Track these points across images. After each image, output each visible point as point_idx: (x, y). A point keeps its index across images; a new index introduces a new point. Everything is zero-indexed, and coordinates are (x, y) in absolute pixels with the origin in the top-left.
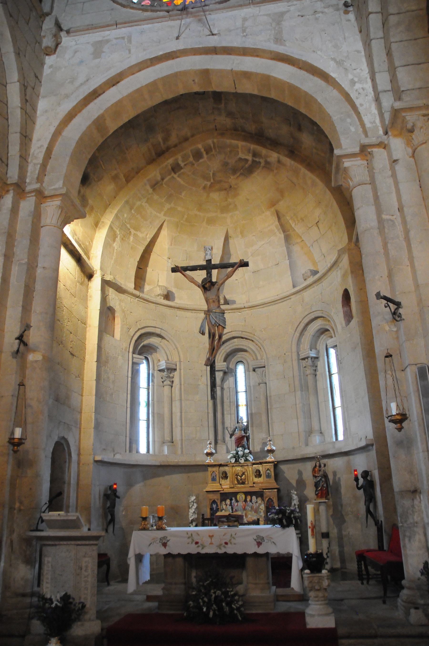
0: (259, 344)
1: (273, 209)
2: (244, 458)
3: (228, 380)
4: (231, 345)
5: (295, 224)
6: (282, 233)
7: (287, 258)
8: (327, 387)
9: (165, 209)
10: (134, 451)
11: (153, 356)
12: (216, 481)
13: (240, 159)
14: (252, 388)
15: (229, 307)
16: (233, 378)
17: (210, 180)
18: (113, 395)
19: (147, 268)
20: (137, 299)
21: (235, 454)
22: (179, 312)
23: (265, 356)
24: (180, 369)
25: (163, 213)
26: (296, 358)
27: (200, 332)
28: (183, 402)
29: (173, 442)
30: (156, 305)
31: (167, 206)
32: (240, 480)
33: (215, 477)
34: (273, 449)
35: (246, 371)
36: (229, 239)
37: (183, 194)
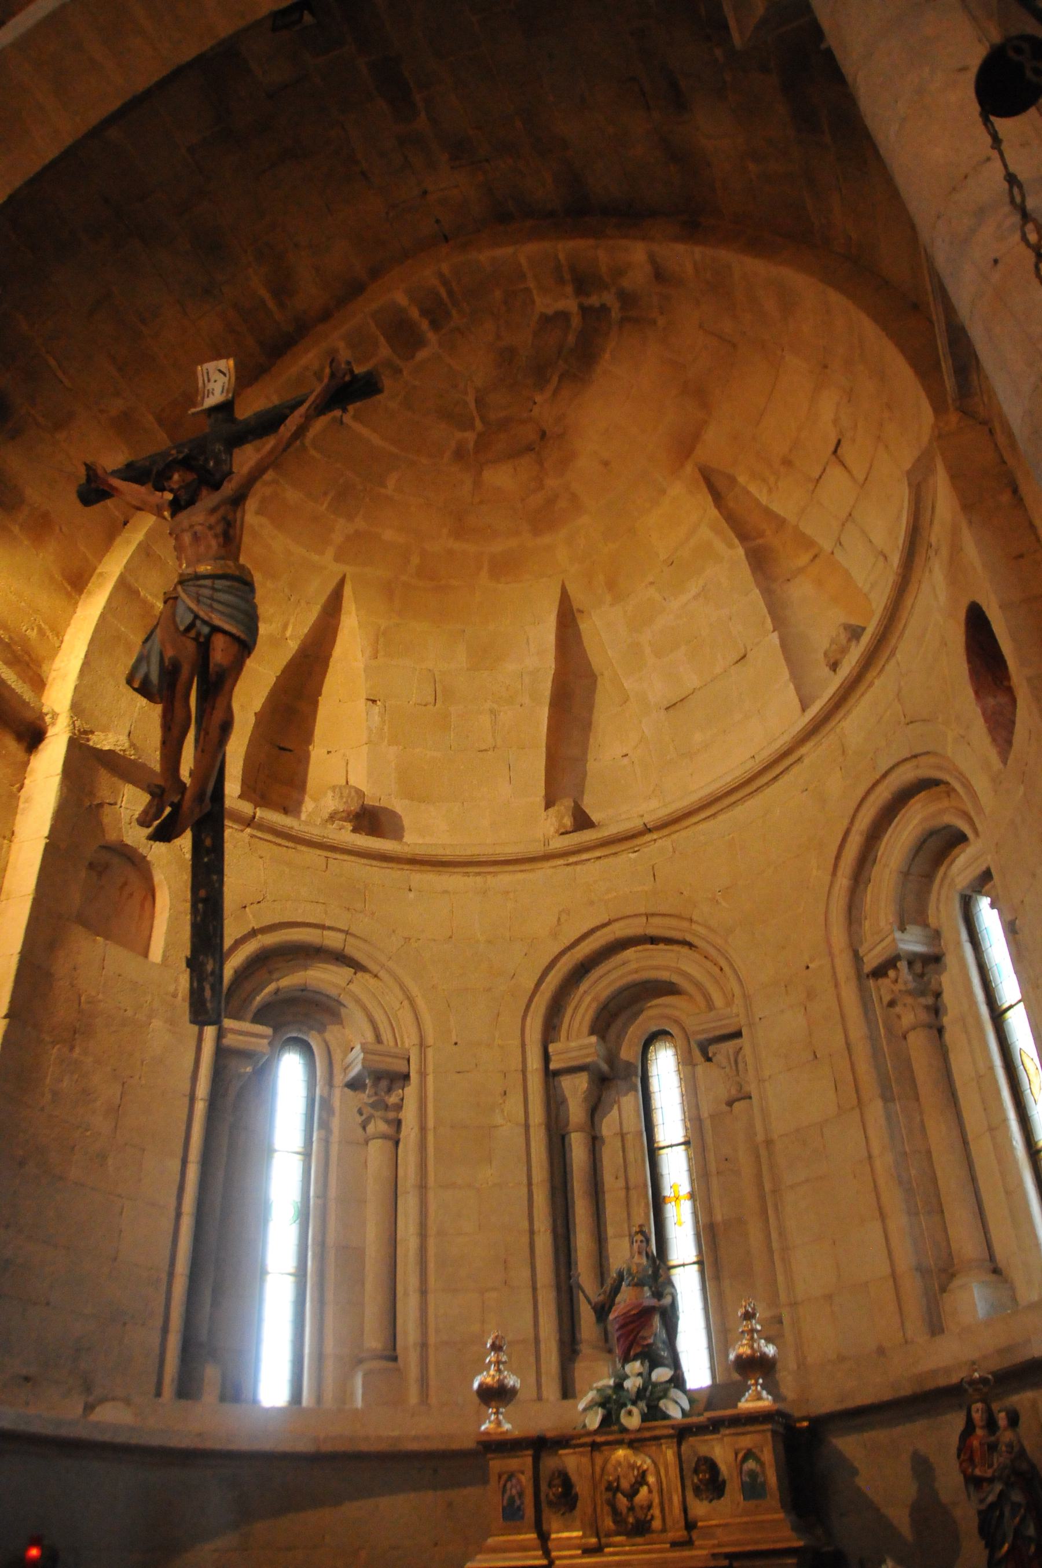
0: (713, 953)
1: (689, 468)
2: (642, 1405)
3: (616, 1107)
4: (613, 976)
5: (770, 491)
6: (736, 541)
7: (769, 624)
8: (991, 1068)
9: (338, 538)
10: (210, 1396)
11: (328, 1035)
12: (522, 1517)
13: (547, 320)
14: (707, 1124)
15: (594, 837)
16: (637, 1098)
17: (472, 427)
18: (110, 1161)
19: (311, 747)
20: (248, 830)
21: (610, 1392)
22: (421, 878)
23: (737, 991)
24: (423, 1074)
25: (330, 552)
26: (852, 973)
27: (129, 681)
28: (431, 1195)
29: (395, 1359)
30: (329, 854)
31: (341, 528)
32: (624, 1511)
33: (518, 1502)
34: (764, 1356)
35: (686, 1062)
36: (579, 621)
37: (391, 482)
